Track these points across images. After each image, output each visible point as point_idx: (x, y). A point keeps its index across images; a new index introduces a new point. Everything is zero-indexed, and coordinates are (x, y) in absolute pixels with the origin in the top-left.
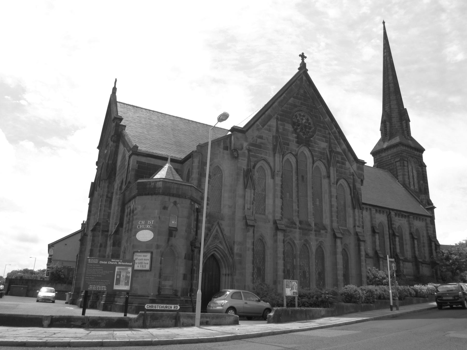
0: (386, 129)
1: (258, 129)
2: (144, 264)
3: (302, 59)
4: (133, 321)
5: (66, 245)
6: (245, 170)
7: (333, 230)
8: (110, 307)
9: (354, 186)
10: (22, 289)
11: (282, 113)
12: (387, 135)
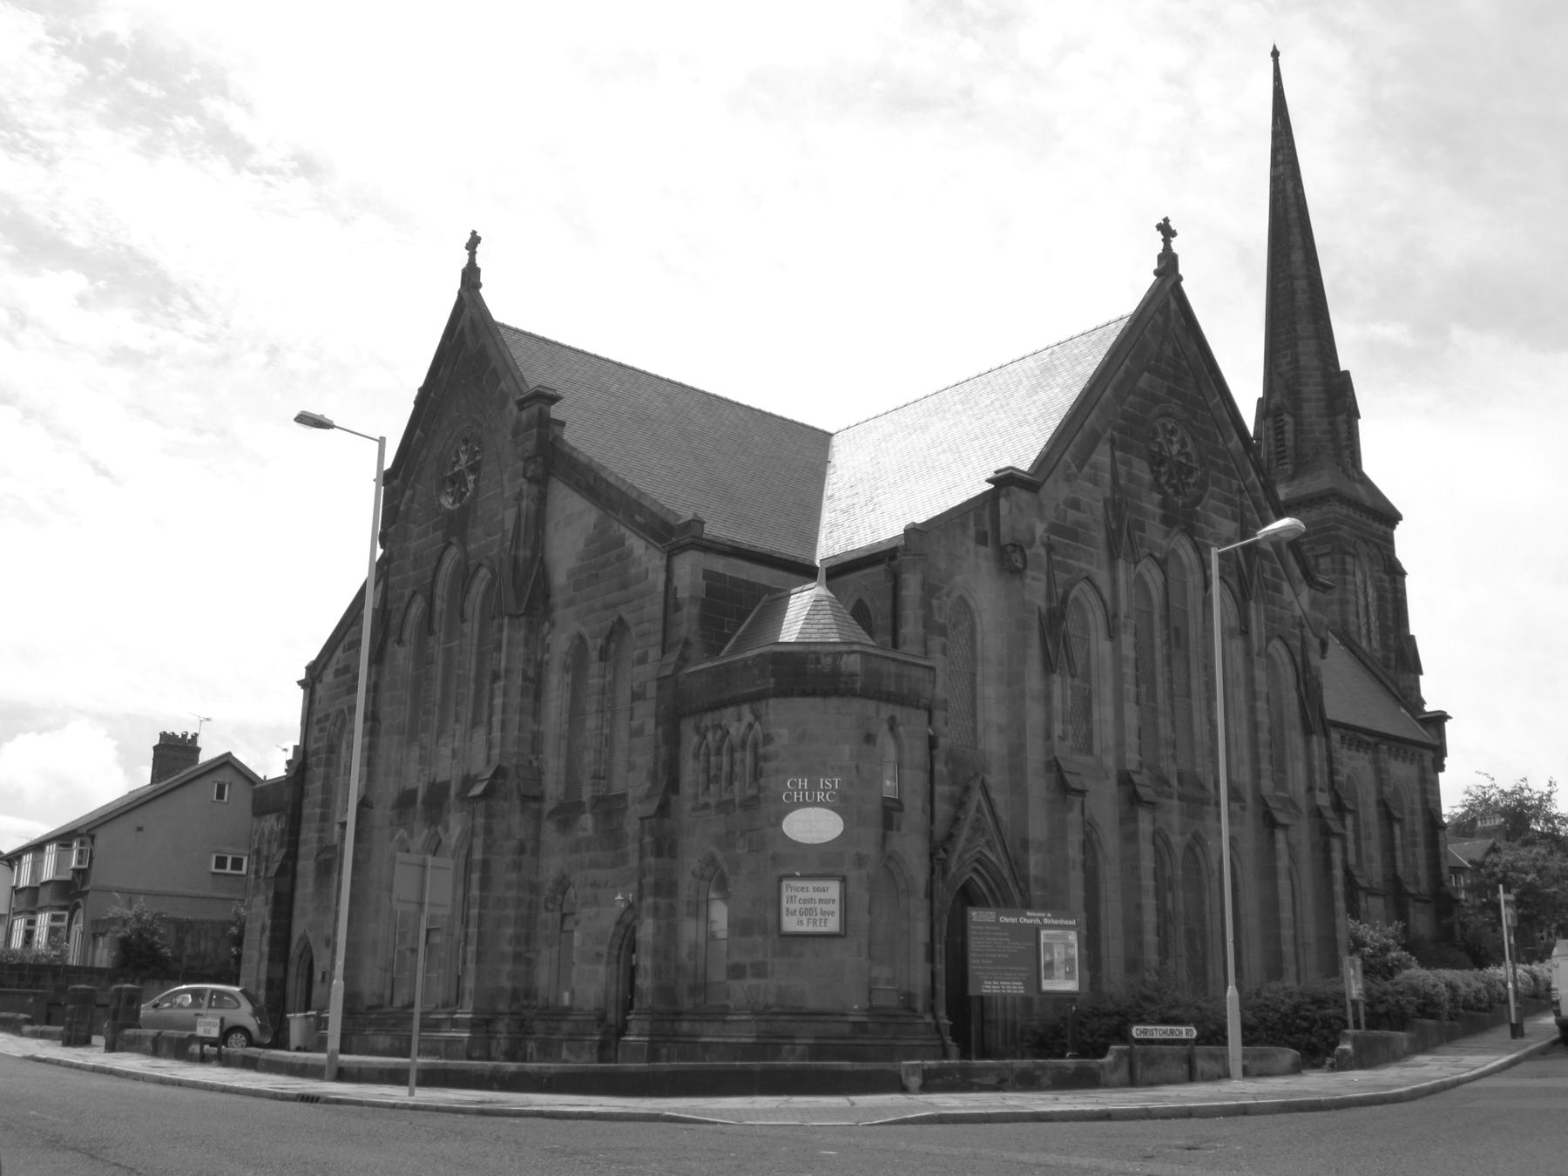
0: (1280, 437)
1: (1069, 479)
2: (819, 914)
3: (1163, 240)
4: (1107, 1069)
5: (140, 829)
6: (1044, 611)
7: (1261, 800)
8: (664, 1051)
9: (1306, 661)
10: (31, 1000)
11: (1123, 422)
12: (1284, 457)
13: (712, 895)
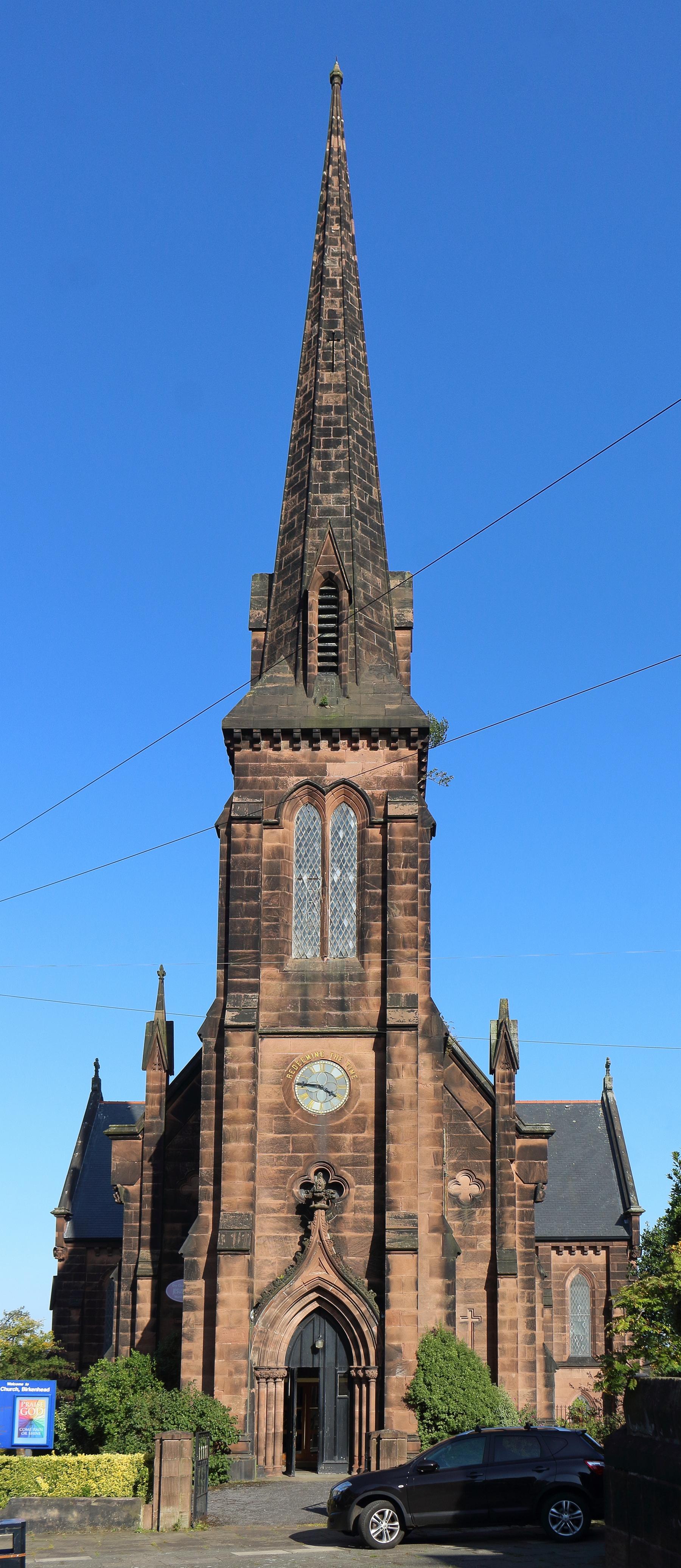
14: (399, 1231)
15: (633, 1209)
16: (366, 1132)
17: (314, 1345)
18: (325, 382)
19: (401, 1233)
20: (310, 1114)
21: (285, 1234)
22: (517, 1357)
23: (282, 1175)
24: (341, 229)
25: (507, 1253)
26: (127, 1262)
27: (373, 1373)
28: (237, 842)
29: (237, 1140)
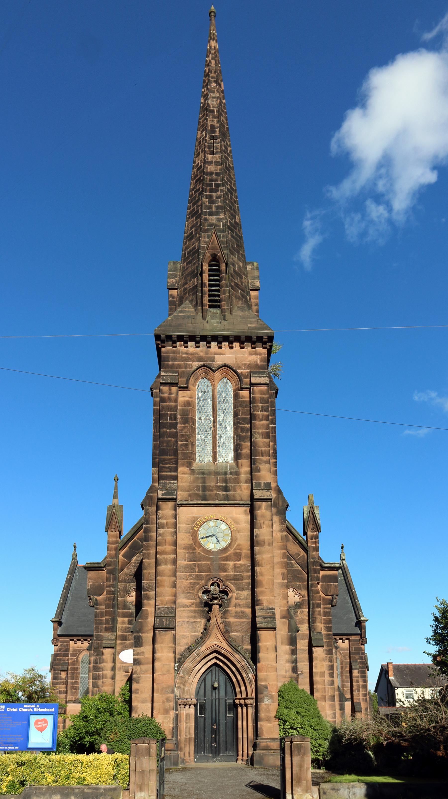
13: (49, 686)
14: (265, 617)
15: (362, 619)
16: (241, 561)
17: (213, 685)
18: (209, 160)
19: (266, 618)
20: (208, 551)
21: (194, 620)
22: (325, 693)
23: (192, 585)
24: (217, 86)
25: (317, 634)
26: (96, 640)
27: (251, 701)
28: (164, 397)
29: (166, 564)
